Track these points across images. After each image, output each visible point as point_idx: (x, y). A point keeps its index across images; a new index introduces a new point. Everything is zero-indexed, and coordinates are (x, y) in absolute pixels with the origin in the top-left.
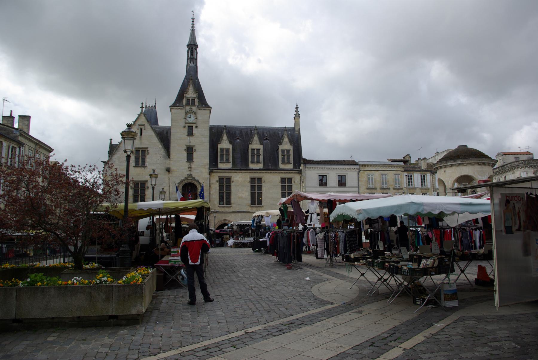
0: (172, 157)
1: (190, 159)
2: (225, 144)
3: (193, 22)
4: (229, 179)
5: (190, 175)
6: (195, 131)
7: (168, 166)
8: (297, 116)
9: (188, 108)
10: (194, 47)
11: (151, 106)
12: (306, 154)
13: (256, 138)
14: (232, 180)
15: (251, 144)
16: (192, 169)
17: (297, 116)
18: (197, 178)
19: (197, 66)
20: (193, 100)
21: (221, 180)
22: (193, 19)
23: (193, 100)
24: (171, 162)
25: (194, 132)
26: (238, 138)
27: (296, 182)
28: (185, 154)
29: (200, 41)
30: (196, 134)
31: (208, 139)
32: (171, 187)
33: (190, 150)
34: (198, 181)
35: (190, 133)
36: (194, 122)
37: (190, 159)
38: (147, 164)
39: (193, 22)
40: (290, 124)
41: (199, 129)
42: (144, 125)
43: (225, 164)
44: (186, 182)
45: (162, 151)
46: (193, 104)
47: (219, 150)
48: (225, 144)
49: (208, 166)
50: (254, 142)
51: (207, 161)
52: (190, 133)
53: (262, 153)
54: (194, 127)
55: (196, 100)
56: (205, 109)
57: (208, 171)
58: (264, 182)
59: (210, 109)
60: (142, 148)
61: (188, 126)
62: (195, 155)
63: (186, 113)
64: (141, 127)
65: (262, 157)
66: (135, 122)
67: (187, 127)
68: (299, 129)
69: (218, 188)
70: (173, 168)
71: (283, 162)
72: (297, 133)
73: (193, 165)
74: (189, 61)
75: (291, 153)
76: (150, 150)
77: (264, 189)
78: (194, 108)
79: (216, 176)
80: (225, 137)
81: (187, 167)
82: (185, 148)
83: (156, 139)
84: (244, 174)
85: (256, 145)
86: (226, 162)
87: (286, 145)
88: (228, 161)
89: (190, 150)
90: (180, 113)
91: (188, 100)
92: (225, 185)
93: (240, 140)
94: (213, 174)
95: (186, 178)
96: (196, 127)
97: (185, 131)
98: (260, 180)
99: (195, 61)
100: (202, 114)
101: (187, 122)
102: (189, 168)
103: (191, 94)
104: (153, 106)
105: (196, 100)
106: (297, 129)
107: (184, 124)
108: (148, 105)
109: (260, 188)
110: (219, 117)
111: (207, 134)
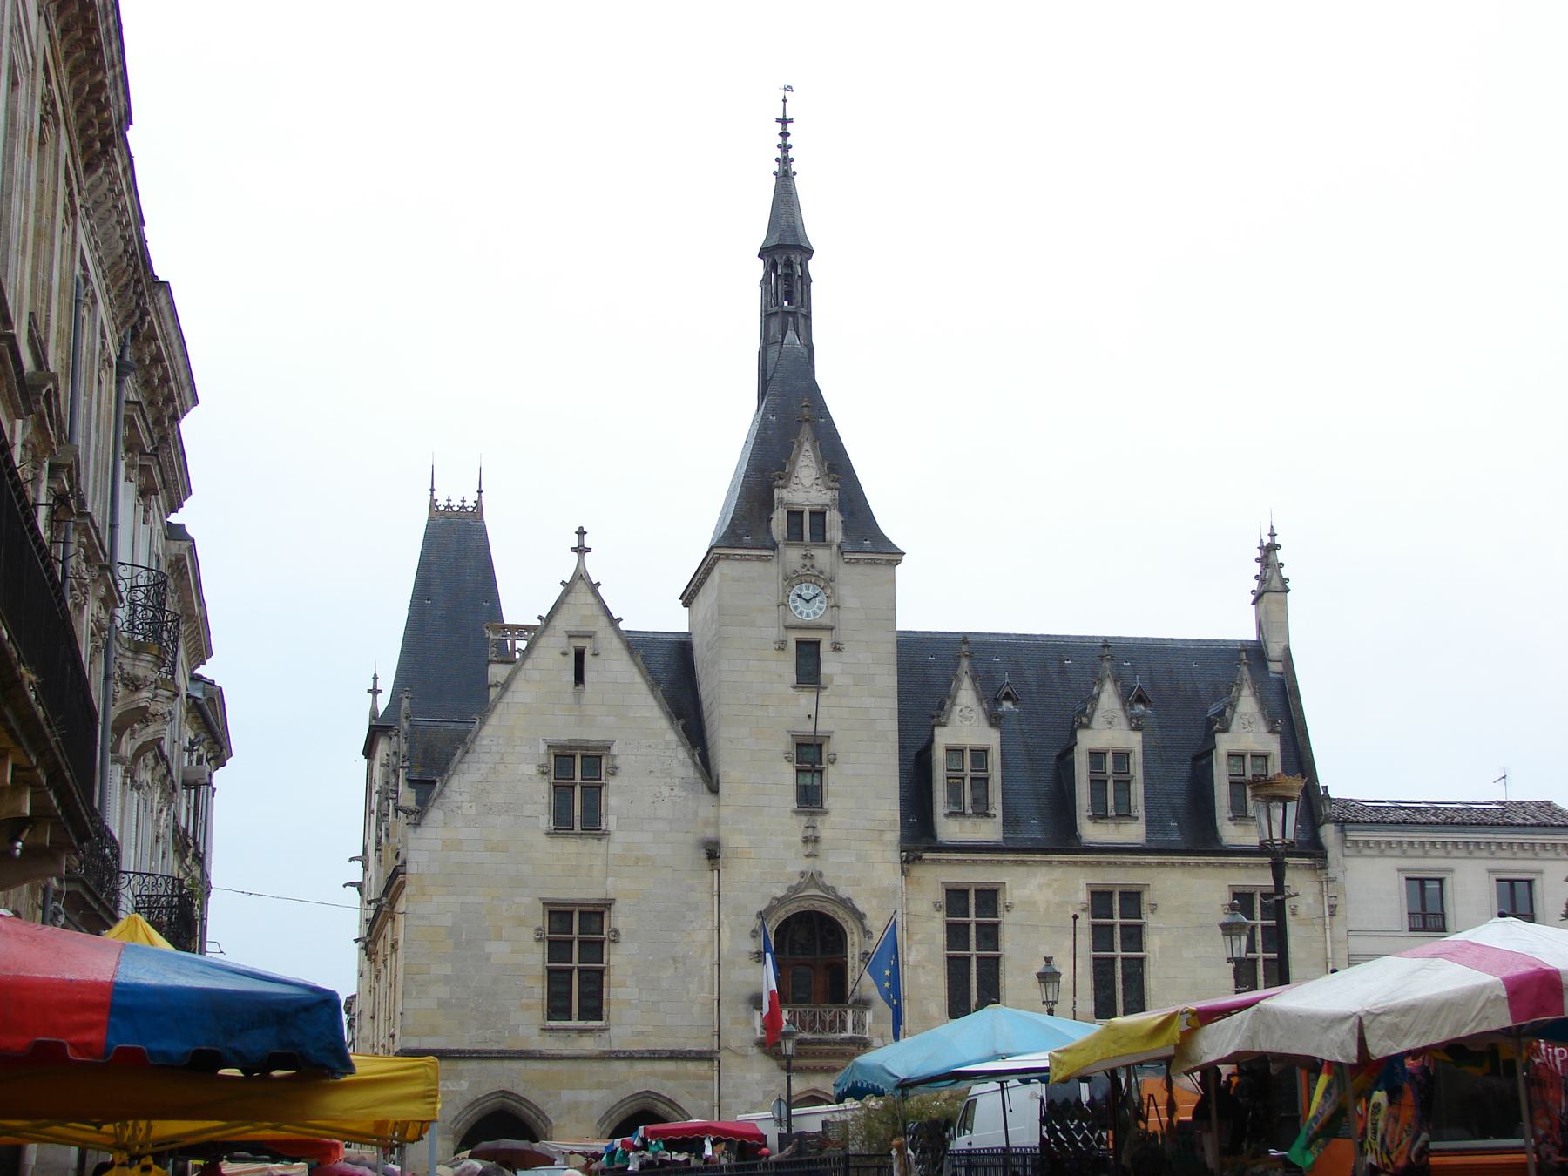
0: (723, 789)
1: (810, 799)
2: (966, 726)
3: (785, 135)
4: (989, 898)
5: (813, 879)
6: (830, 665)
7: (710, 833)
8: (1271, 586)
9: (793, 555)
10: (796, 258)
11: (456, 503)
12: (1342, 773)
13: (1108, 699)
14: (1003, 899)
15: (1087, 727)
16: (823, 846)
17: (1271, 586)
18: (843, 892)
19: (811, 350)
20: (819, 516)
21: (955, 898)
22: (784, 121)
23: (819, 516)
24: (725, 812)
25: (825, 669)
26: (1008, 697)
27: (1302, 909)
28: (788, 773)
29: (815, 229)
30: (838, 680)
31: (892, 703)
32: (725, 932)
33: (810, 755)
34: (846, 904)
35: (808, 670)
36: (826, 621)
37: (810, 799)
38: (610, 821)
39: (785, 135)
40: (1240, 626)
41: (845, 656)
42: (590, 636)
43: (968, 824)
44: (793, 908)
45: (678, 758)
46: (819, 535)
47: (939, 755)
48: (966, 726)
49: (894, 835)
50: (1098, 720)
51: (888, 809)
52: (808, 670)
53: (995, 758)
54: (825, 648)
55: (834, 518)
56: (874, 562)
57: (893, 855)
58: (1154, 908)
59: (892, 555)
60: (583, 746)
61: (799, 643)
62: (834, 780)
63: (791, 580)
64: (580, 643)
65: (1138, 790)
66: (547, 620)
67: (792, 646)
68: (1287, 650)
69: (941, 938)
70: (732, 840)
71: (1099, 815)
72: (1275, 667)
73: (827, 829)
74: (775, 324)
75: (995, 758)
76: (622, 754)
77: (1153, 944)
78: (823, 557)
79: (936, 877)
80: (966, 695)
81: (798, 839)
82: (785, 744)
83: (651, 701)
84: (1058, 873)
85: (1109, 729)
86: (976, 814)
87: (1247, 734)
88: (982, 811)
89: (810, 755)
90: (752, 580)
91: (795, 516)
92: (973, 924)
93: (1015, 701)
94: (918, 871)
95: (795, 889)
96: (837, 648)
97: (787, 666)
98: (1132, 899)
99: (801, 321)
100: (852, 581)
101: (791, 621)
102: (806, 841)
103: (806, 486)
104: (470, 503)
105: (834, 518)
106: (1274, 650)
107: (774, 633)
108: (442, 502)
109: (1134, 936)
110: (936, 595)
111: (888, 679)
